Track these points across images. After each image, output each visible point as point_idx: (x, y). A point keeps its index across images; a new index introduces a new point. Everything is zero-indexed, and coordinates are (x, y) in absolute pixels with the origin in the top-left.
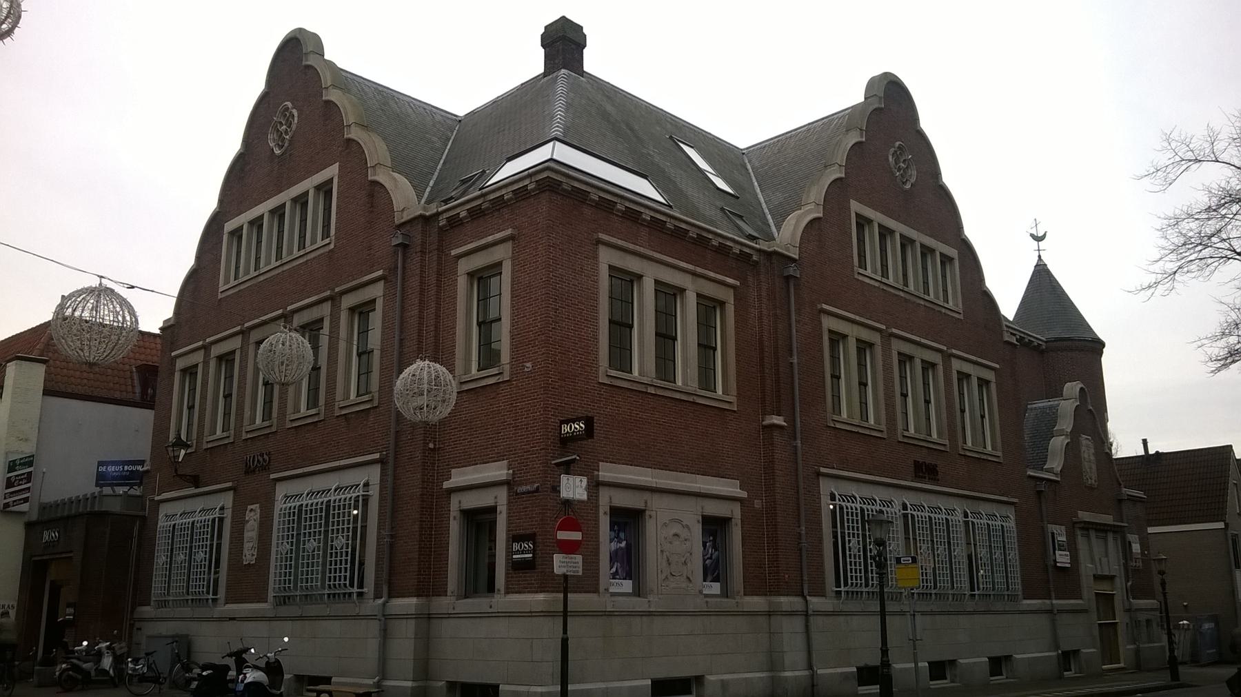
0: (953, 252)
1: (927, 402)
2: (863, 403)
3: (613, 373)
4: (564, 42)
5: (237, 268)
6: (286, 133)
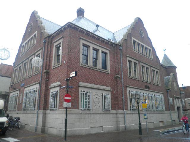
0: (151, 49)
2: (135, 74)
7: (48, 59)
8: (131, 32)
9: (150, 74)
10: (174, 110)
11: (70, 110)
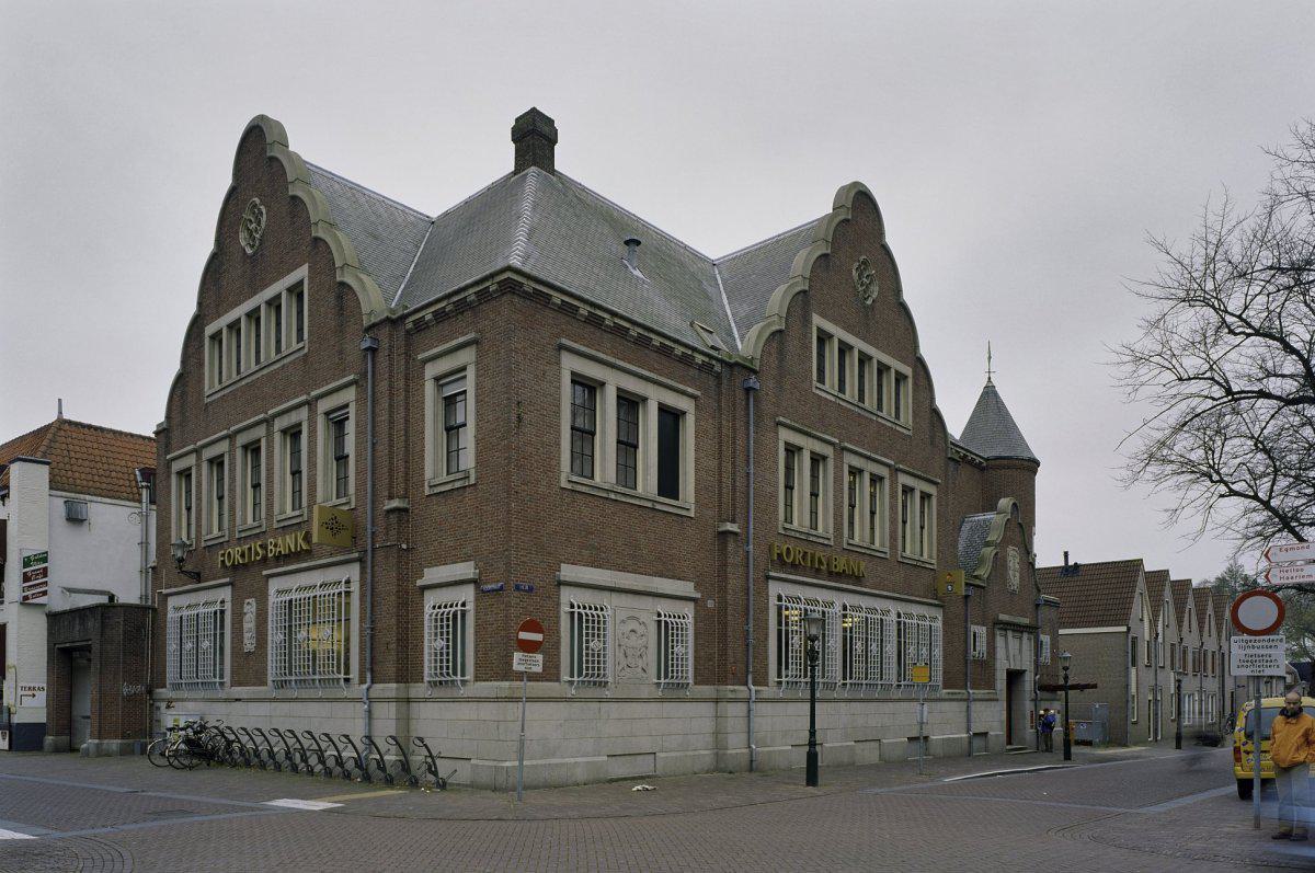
0: (907, 371)
1: (922, 528)
2: (814, 513)
3: (575, 479)
4: (534, 137)
5: (220, 373)
6: (256, 231)
7: (399, 444)
8: (810, 280)
9: (887, 513)
10: (990, 684)
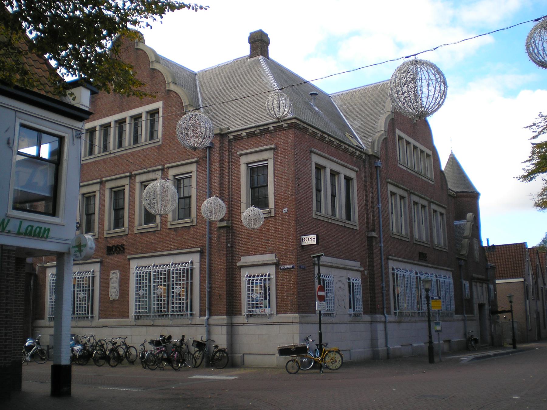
0: (430, 153)
4: (259, 42)
10: (471, 311)
11: (307, 316)
